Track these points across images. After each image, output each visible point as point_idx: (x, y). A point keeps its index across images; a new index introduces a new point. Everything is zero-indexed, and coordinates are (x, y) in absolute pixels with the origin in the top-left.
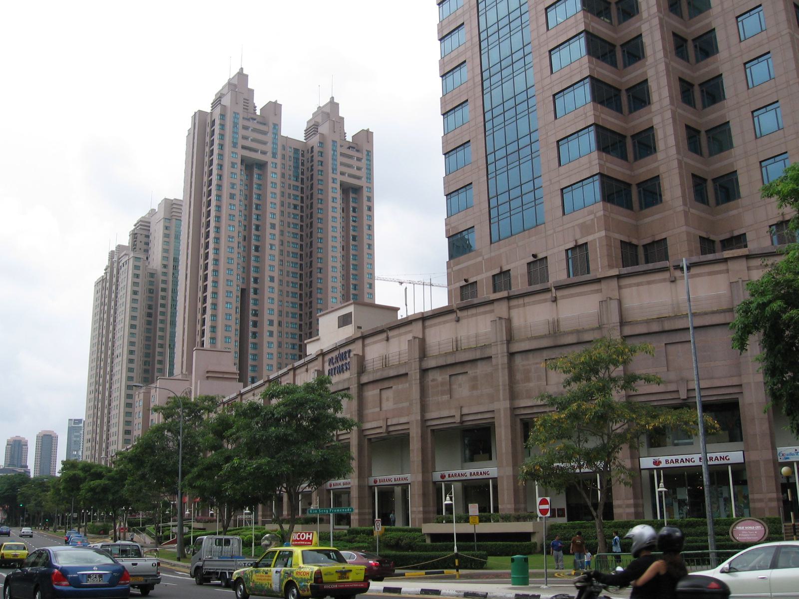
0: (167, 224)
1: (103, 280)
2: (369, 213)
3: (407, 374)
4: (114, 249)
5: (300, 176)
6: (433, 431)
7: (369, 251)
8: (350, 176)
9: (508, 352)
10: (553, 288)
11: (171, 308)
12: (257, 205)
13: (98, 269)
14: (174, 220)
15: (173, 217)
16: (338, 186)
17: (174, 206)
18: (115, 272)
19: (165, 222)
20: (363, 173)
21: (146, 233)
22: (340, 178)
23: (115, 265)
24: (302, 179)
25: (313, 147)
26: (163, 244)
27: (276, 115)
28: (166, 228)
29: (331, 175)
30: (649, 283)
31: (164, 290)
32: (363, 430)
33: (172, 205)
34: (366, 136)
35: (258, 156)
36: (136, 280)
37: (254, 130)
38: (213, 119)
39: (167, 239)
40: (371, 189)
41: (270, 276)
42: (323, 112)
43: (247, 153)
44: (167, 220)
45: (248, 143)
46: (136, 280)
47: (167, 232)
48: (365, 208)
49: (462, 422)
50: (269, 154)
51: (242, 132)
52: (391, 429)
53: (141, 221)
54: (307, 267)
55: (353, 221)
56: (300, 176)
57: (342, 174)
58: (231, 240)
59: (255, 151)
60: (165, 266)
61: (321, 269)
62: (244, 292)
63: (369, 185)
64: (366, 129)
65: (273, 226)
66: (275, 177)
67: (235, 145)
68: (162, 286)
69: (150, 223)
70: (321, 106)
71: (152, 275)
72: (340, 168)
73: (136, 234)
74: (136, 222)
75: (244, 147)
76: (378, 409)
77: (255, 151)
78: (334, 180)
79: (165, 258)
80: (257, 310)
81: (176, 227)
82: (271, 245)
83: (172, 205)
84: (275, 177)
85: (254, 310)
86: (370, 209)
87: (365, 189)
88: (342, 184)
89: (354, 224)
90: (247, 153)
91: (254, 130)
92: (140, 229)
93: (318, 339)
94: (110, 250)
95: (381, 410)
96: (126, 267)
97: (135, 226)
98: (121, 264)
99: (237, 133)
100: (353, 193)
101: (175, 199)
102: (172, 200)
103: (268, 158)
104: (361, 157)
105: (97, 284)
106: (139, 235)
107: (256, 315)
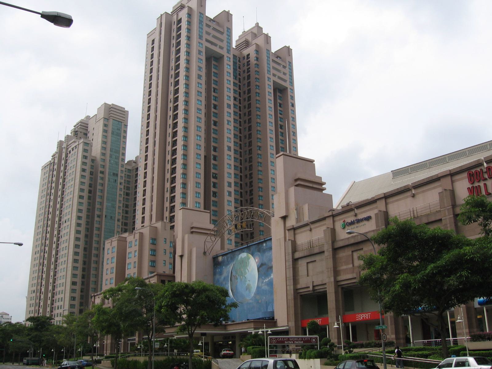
0: (106, 123)
1: (50, 164)
2: (293, 108)
3: (441, 220)
4: (63, 139)
5: (238, 77)
6: (301, 296)
7: (294, 138)
8: (279, 78)
9: (454, 214)
10: (484, 163)
11: (108, 187)
12: (215, 89)
13: (47, 152)
14: (112, 120)
15: (111, 117)
16: (272, 84)
17: (112, 109)
18: (64, 156)
19: (104, 121)
20: (287, 77)
21: (85, 132)
22: (273, 78)
23: (64, 150)
24: (240, 79)
25: (249, 55)
26: (103, 138)
27: (229, 21)
28: (105, 125)
29: (267, 75)
30: (423, 192)
31: (102, 172)
32: (297, 289)
33: (110, 108)
34: (288, 51)
35: (217, 49)
36: (85, 160)
37: (214, 29)
38: (179, 18)
39: (105, 134)
40: (293, 90)
41: (228, 146)
42: (252, 32)
43: (209, 45)
44: (106, 120)
45: (210, 38)
46: (85, 160)
47: (106, 128)
48: (290, 104)
49: (314, 290)
50: (225, 50)
51: (205, 28)
52: (316, 288)
53: (81, 122)
54: (246, 146)
55: (280, 114)
56: (238, 77)
57: (274, 75)
58: (199, 112)
59: (216, 45)
60: (103, 154)
61: (260, 147)
62: (207, 159)
63: (292, 88)
64: (287, 46)
65: (229, 106)
66: (228, 67)
67: (201, 37)
68: (100, 169)
69: (88, 124)
70: (246, 31)
71: (93, 161)
72: (273, 71)
73: (77, 131)
74: (75, 124)
75: (207, 41)
76: (351, 266)
77: (216, 45)
78: (269, 78)
79: (104, 148)
80: (217, 174)
81: (113, 125)
82: (228, 121)
83: (110, 108)
84: (228, 67)
85: (215, 173)
86: (293, 105)
87: (289, 90)
88: (274, 82)
89: (280, 116)
90: (209, 45)
91: (214, 29)
92: (80, 128)
93: (210, 223)
94: (66, 135)
95: (353, 266)
96: (75, 150)
97: (74, 126)
98: (69, 149)
99: (202, 29)
100: (279, 92)
101: (112, 104)
102: (110, 105)
103: (224, 52)
104: (285, 65)
105: (44, 168)
106: (79, 133)
107: (215, 177)
